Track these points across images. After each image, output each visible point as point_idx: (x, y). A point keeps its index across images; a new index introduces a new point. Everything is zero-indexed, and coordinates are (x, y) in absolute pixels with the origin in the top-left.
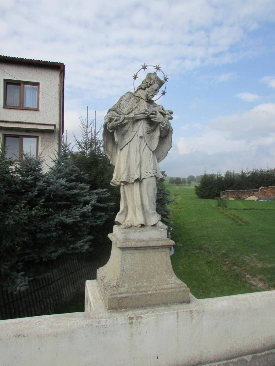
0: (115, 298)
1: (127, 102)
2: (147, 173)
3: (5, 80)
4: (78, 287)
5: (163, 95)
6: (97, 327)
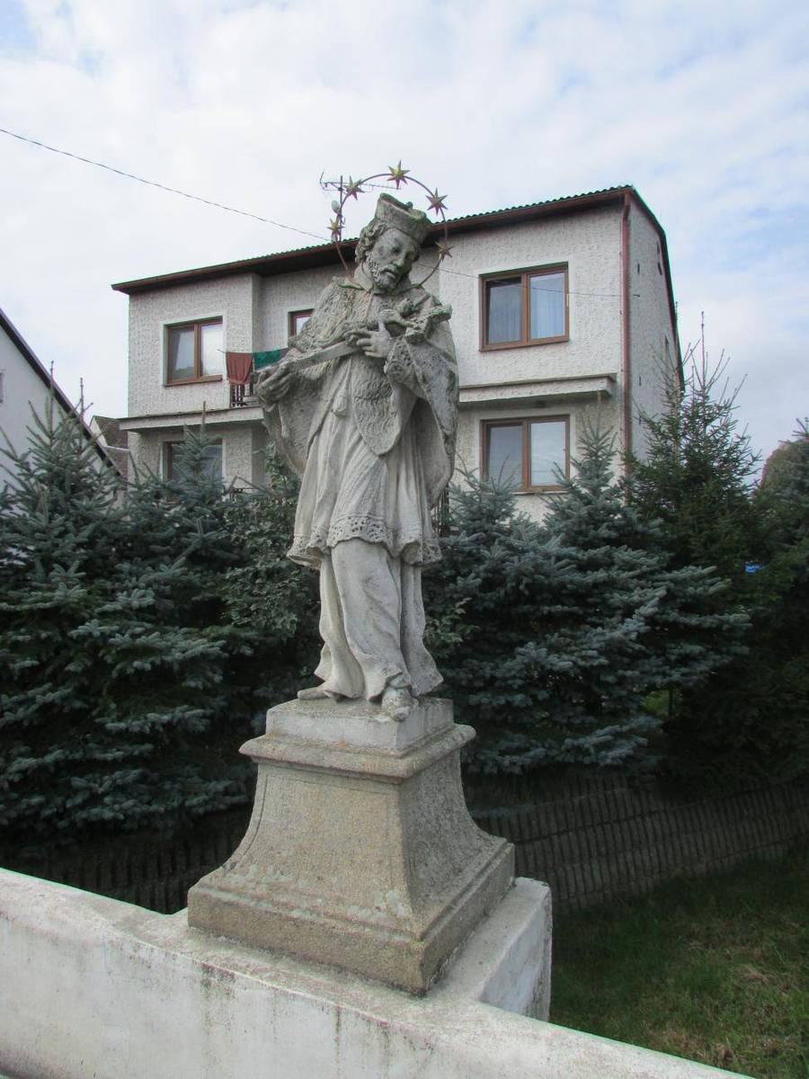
0: (205, 896)
1: (325, 311)
3: (483, 277)
4: (625, 873)
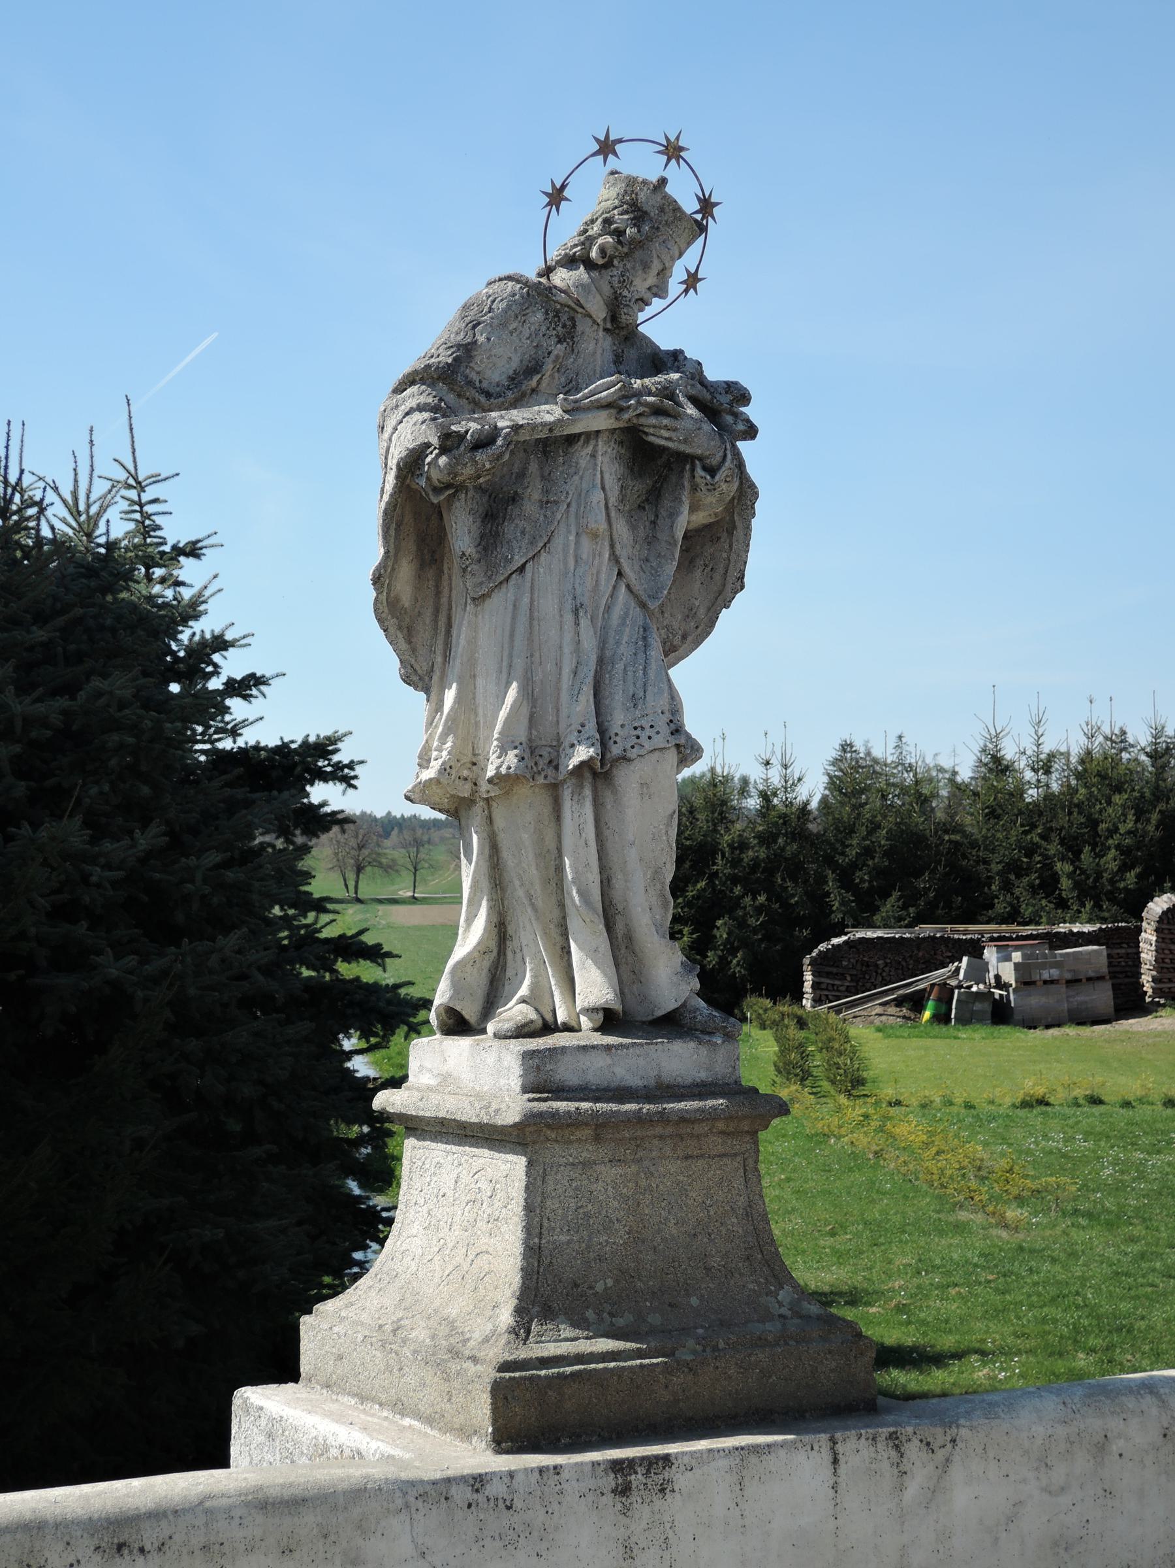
2: (638, 732)
5: (686, 291)
6: (470, 1506)
